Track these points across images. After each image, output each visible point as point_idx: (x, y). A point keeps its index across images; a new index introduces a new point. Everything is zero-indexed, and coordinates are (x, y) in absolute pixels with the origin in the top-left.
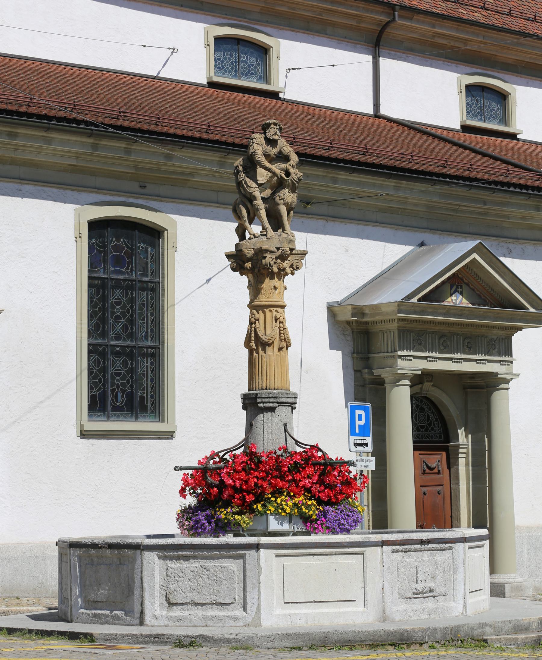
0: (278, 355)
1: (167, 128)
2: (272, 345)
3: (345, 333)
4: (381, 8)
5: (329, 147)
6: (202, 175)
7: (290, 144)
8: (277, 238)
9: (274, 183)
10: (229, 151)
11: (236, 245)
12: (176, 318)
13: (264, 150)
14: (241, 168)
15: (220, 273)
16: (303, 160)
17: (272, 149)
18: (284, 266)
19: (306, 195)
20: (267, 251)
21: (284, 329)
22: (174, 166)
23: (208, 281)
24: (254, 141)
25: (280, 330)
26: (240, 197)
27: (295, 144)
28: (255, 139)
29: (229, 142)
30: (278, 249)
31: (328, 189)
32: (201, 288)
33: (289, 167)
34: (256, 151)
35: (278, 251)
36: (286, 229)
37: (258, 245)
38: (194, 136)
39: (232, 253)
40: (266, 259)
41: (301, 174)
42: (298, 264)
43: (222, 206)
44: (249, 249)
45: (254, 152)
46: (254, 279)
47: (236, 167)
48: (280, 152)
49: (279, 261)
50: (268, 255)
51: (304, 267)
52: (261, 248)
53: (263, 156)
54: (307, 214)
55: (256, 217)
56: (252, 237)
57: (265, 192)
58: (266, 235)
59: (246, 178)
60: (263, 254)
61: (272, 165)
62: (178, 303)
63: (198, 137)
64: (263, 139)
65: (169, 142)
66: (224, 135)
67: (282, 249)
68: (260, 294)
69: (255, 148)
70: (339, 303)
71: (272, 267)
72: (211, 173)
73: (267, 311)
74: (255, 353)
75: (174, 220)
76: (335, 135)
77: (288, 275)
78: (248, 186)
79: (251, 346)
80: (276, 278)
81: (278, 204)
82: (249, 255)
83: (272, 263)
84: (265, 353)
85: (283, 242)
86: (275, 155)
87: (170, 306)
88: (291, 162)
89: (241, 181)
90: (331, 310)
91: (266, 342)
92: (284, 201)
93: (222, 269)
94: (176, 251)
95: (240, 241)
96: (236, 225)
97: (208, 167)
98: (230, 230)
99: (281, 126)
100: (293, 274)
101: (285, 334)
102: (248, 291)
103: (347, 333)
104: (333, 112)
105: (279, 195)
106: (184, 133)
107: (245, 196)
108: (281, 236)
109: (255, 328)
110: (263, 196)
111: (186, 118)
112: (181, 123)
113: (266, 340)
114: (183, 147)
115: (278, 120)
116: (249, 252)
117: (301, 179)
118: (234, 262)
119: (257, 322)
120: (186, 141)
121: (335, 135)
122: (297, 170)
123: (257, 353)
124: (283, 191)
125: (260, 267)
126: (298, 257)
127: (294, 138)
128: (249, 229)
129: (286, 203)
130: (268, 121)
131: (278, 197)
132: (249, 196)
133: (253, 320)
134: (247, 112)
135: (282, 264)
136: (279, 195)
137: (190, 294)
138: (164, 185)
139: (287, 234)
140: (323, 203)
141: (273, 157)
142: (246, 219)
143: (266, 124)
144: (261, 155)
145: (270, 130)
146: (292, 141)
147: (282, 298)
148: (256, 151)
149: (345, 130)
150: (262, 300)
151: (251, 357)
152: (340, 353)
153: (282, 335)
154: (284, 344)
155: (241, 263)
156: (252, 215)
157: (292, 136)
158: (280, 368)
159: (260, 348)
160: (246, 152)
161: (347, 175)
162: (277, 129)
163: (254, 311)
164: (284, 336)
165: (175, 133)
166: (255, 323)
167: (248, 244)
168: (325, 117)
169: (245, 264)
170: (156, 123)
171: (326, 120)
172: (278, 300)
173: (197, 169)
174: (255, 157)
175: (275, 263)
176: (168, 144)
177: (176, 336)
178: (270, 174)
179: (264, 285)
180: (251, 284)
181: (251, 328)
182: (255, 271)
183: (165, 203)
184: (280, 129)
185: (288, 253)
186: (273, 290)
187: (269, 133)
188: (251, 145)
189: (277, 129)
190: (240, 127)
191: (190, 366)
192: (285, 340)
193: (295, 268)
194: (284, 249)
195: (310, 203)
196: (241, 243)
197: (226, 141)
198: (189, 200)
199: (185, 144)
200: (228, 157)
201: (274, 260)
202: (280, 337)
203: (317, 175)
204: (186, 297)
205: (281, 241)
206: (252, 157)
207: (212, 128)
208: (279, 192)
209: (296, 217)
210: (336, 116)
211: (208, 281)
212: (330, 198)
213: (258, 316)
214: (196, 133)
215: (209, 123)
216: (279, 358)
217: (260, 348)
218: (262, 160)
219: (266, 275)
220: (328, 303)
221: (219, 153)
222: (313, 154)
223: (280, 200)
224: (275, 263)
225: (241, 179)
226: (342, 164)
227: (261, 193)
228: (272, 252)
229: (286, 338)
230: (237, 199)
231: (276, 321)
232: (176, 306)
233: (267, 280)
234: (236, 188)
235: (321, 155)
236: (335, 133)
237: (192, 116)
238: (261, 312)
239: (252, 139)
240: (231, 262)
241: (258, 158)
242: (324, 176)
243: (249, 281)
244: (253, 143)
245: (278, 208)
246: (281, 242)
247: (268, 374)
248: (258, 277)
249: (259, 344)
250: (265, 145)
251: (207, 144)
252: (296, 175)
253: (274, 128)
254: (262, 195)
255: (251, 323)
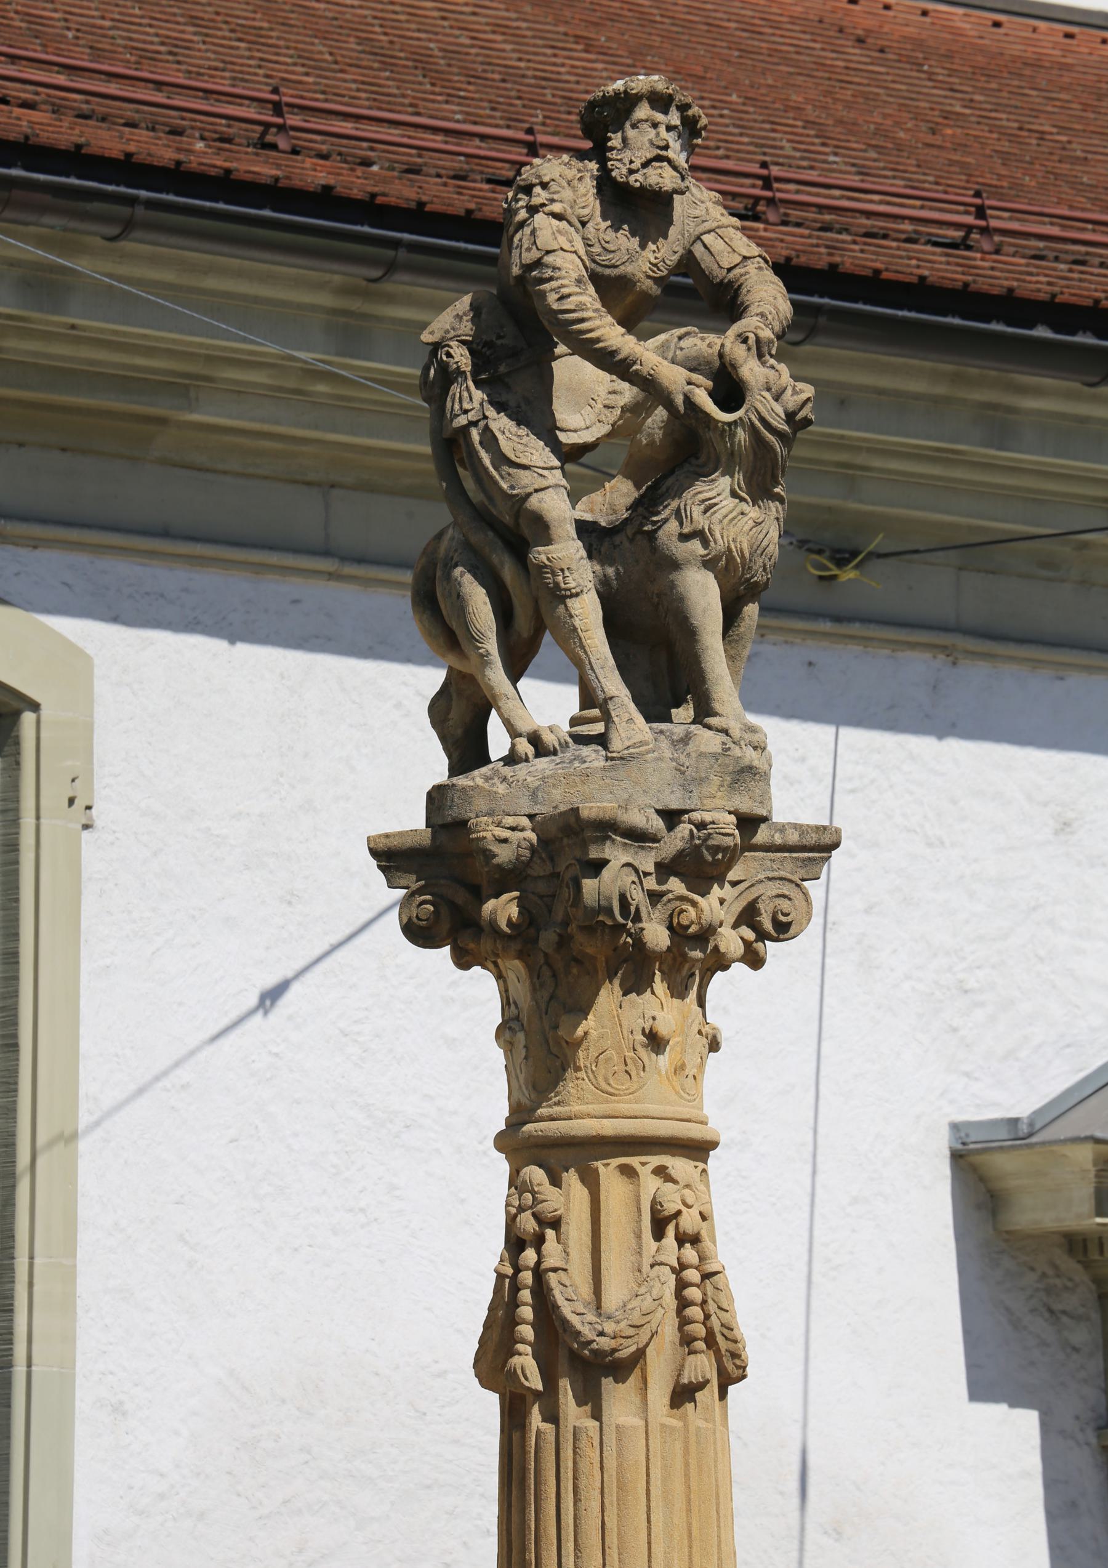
0: (672, 1429)
1: (35, 116)
2: (637, 1371)
3: (1058, 1307)
4: (321, 286)
5: (969, 228)
6: (239, 392)
7: (741, 217)
8: (668, 754)
9: (651, 443)
10: (391, 253)
11: (430, 796)
12: (85, 1211)
13: (597, 249)
14: (461, 357)
15: (339, 955)
16: (818, 309)
17: (643, 246)
18: (706, 918)
19: (830, 509)
20: (606, 828)
21: (707, 1276)
22: (74, 336)
23: (272, 996)
24: (536, 201)
25: (682, 1285)
26: (455, 524)
27: (772, 216)
28: (544, 186)
29: (392, 200)
30: (671, 817)
31: (959, 473)
32: (233, 1037)
33: (738, 352)
34: (549, 259)
35: (671, 827)
36: (717, 706)
37: (557, 794)
38: (193, 163)
39: (409, 843)
40: (605, 873)
41: (808, 391)
42: (785, 905)
43: (349, 569)
44: (510, 821)
45: (538, 264)
46: (534, 990)
47: (436, 346)
48: (688, 263)
49: (676, 886)
50: (617, 854)
51: (817, 920)
52: (575, 811)
53: (591, 289)
54: (838, 619)
55: (547, 637)
56: (525, 747)
57: (597, 497)
58: (602, 740)
59: (491, 412)
60: (584, 846)
61: (643, 337)
62: (97, 1124)
63: (213, 172)
64: (588, 187)
65: (48, 199)
66: (367, 163)
67: (697, 816)
68: (570, 1074)
69: (545, 239)
70: (1024, 1129)
71: (637, 918)
72: (291, 383)
73: (607, 1170)
74: (536, 1418)
75: (80, 653)
76: (1006, 158)
77: (725, 967)
78: (502, 460)
79: (513, 1374)
80: (660, 986)
81: (675, 565)
82: (504, 855)
83: (638, 897)
84: (597, 1415)
85: (702, 781)
86: (656, 280)
87: (51, 1144)
88: (749, 323)
89: (465, 430)
90: (974, 1169)
91: (598, 1353)
92: (705, 543)
93: (348, 931)
94: (86, 827)
95: (454, 771)
96: (433, 678)
97: (272, 349)
98: (398, 705)
99: (695, 110)
100: (755, 960)
101: (712, 1307)
102: (497, 1056)
103: (1071, 1302)
104: (997, 24)
105: (678, 513)
106: (132, 148)
107: (483, 517)
108: (691, 747)
109: (539, 1273)
110: (588, 517)
111: (147, 56)
112: (113, 88)
113: (604, 1343)
114: (128, 226)
115: (676, 74)
116: (507, 834)
117: (807, 422)
118: (420, 891)
119: (550, 1233)
120: (143, 194)
121: (1006, 158)
122: (783, 367)
123: (552, 1416)
124: (699, 486)
125: (566, 923)
126: (785, 865)
127: (767, 182)
128: (510, 705)
129: (717, 559)
130: (619, 85)
131: (673, 526)
132: (507, 519)
133: (528, 1223)
134: (498, 28)
135: (694, 904)
136: (678, 513)
137: (165, 1073)
138: (21, 445)
139: (725, 732)
140: (928, 556)
141: (645, 295)
142: (491, 645)
143: (607, 101)
144: (579, 281)
145: (631, 133)
146: (757, 199)
147: (696, 1098)
148: (549, 259)
149: (1062, 129)
150: (576, 1108)
151: (516, 1436)
152: (1028, 1421)
153: (695, 1312)
154: (702, 1366)
155: (461, 897)
156: (523, 623)
157: (755, 169)
158: (679, 1504)
159: (565, 1385)
160: (492, 260)
161: (1069, 395)
162: (669, 128)
163: (536, 1174)
164: (707, 1317)
165: (79, 147)
166: (539, 1241)
167: (501, 789)
168: (949, 56)
169: (482, 901)
170: (756, 204)
171: (952, 72)
172: (670, 1111)
173: (210, 359)
174: (543, 295)
175: (655, 897)
176: (44, 209)
177: (83, 1319)
178: (628, 393)
179: (589, 1024)
180: (517, 1018)
181: (517, 1270)
182: (542, 944)
183: (23, 552)
184: (690, 128)
185: (729, 841)
186: (643, 1053)
187: (626, 155)
188: (522, 225)
189: (669, 128)
190: (455, 117)
191: (162, 1496)
192: (710, 1340)
193: (768, 925)
194: (708, 817)
195: (854, 554)
196: (461, 781)
197: (373, 196)
198: (166, 533)
199: (140, 212)
200: (388, 287)
201: (651, 883)
202: (684, 1321)
203: (896, 393)
204: (140, 1091)
205: (690, 773)
206: (527, 294)
207: (293, 120)
208: (678, 494)
209: (771, 637)
210: (1016, 49)
211: (272, 996)
212: (972, 529)
213: (553, 1199)
214: (200, 145)
215: (276, 91)
216: (678, 1446)
217: (565, 1385)
218: (581, 307)
219: (601, 964)
220: (955, 1127)
221: (335, 266)
222: (877, 272)
223: (684, 538)
224: (655, 897)
225: (462, 420)
226: (1042, 332)
227: (574, 497)
228: (638, 837)
229: (717, 1327)
230: (440, 536)
231: (659, 1234)
232: (83, 1145)
233: (608, 996)
234: (431, 466)
235: (922, 278)
236: (1005, 146)
237: (177, 47)
238: (571, 1178)
239: (528, 190)
240: (400, 893)
241: (562, 298)
242: (936, 400)
243: (507, 1002)
244: (533, 210)
245: (672, 586)
246: (688, 781)
247: (612, 1539)
248: (554, 976)
249: (563, 1364)
250: (599, 225)
251: (267, 213)
252: (777, 398)
253: (655, 125)
254: (583, 512)
255: (515, 1244)
